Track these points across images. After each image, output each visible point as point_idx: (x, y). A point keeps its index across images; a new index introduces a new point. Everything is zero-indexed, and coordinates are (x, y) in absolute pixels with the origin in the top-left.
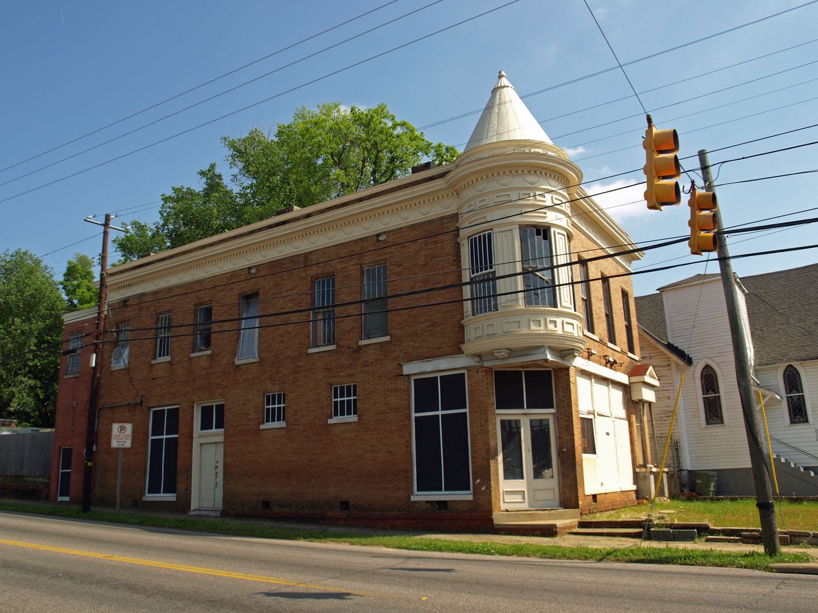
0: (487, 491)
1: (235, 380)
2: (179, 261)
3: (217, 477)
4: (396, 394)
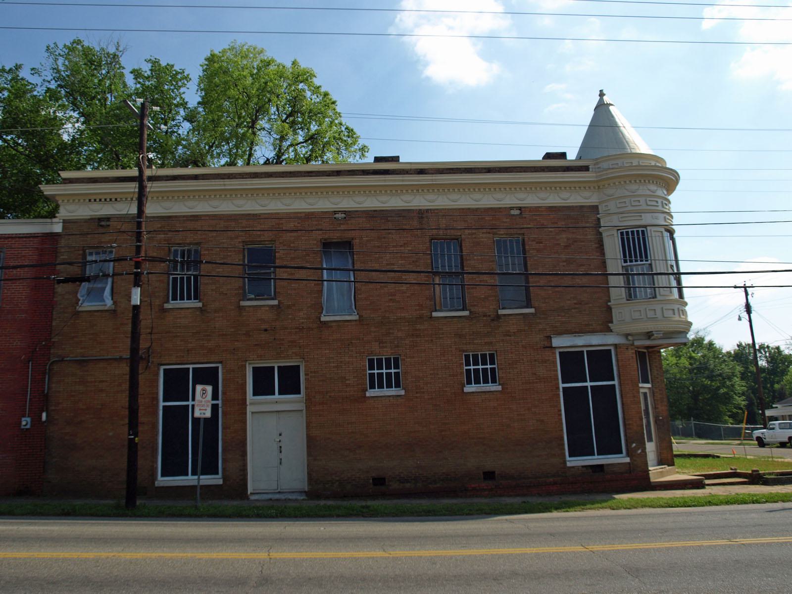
0: (643, 454)
1: (320, 338)
2: (225, 185)
3: (281, 452)
4: (544, 364)
